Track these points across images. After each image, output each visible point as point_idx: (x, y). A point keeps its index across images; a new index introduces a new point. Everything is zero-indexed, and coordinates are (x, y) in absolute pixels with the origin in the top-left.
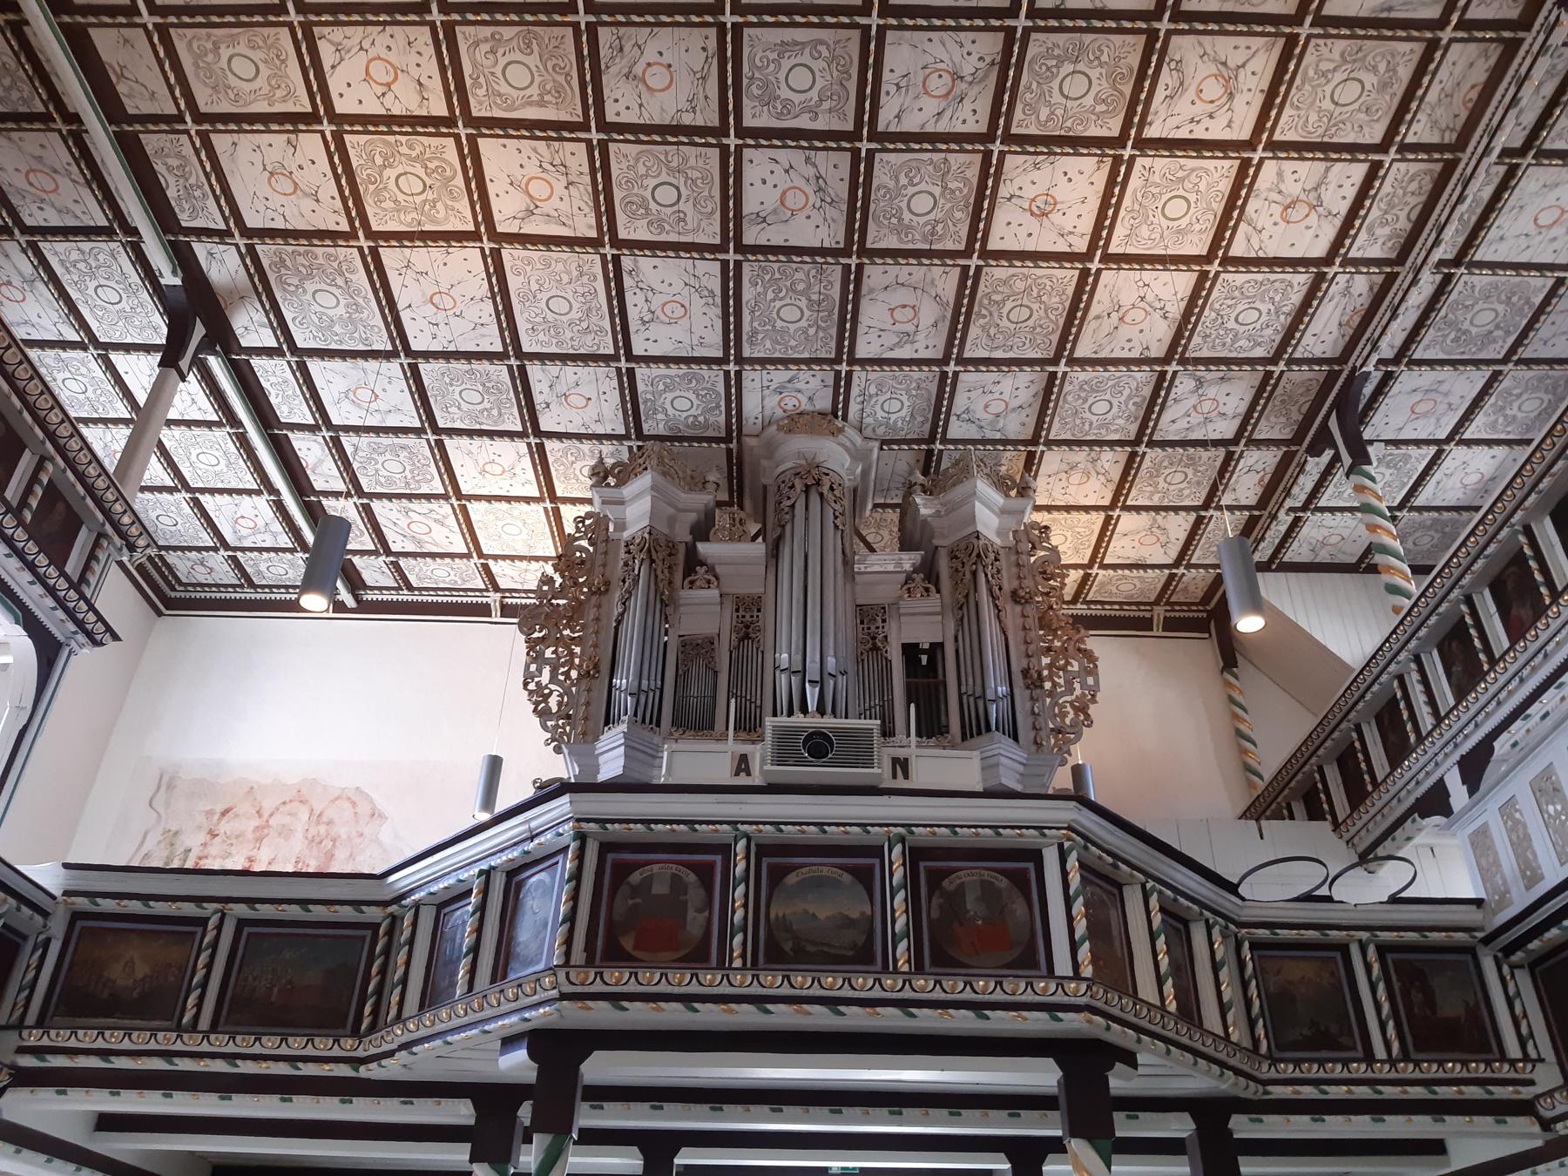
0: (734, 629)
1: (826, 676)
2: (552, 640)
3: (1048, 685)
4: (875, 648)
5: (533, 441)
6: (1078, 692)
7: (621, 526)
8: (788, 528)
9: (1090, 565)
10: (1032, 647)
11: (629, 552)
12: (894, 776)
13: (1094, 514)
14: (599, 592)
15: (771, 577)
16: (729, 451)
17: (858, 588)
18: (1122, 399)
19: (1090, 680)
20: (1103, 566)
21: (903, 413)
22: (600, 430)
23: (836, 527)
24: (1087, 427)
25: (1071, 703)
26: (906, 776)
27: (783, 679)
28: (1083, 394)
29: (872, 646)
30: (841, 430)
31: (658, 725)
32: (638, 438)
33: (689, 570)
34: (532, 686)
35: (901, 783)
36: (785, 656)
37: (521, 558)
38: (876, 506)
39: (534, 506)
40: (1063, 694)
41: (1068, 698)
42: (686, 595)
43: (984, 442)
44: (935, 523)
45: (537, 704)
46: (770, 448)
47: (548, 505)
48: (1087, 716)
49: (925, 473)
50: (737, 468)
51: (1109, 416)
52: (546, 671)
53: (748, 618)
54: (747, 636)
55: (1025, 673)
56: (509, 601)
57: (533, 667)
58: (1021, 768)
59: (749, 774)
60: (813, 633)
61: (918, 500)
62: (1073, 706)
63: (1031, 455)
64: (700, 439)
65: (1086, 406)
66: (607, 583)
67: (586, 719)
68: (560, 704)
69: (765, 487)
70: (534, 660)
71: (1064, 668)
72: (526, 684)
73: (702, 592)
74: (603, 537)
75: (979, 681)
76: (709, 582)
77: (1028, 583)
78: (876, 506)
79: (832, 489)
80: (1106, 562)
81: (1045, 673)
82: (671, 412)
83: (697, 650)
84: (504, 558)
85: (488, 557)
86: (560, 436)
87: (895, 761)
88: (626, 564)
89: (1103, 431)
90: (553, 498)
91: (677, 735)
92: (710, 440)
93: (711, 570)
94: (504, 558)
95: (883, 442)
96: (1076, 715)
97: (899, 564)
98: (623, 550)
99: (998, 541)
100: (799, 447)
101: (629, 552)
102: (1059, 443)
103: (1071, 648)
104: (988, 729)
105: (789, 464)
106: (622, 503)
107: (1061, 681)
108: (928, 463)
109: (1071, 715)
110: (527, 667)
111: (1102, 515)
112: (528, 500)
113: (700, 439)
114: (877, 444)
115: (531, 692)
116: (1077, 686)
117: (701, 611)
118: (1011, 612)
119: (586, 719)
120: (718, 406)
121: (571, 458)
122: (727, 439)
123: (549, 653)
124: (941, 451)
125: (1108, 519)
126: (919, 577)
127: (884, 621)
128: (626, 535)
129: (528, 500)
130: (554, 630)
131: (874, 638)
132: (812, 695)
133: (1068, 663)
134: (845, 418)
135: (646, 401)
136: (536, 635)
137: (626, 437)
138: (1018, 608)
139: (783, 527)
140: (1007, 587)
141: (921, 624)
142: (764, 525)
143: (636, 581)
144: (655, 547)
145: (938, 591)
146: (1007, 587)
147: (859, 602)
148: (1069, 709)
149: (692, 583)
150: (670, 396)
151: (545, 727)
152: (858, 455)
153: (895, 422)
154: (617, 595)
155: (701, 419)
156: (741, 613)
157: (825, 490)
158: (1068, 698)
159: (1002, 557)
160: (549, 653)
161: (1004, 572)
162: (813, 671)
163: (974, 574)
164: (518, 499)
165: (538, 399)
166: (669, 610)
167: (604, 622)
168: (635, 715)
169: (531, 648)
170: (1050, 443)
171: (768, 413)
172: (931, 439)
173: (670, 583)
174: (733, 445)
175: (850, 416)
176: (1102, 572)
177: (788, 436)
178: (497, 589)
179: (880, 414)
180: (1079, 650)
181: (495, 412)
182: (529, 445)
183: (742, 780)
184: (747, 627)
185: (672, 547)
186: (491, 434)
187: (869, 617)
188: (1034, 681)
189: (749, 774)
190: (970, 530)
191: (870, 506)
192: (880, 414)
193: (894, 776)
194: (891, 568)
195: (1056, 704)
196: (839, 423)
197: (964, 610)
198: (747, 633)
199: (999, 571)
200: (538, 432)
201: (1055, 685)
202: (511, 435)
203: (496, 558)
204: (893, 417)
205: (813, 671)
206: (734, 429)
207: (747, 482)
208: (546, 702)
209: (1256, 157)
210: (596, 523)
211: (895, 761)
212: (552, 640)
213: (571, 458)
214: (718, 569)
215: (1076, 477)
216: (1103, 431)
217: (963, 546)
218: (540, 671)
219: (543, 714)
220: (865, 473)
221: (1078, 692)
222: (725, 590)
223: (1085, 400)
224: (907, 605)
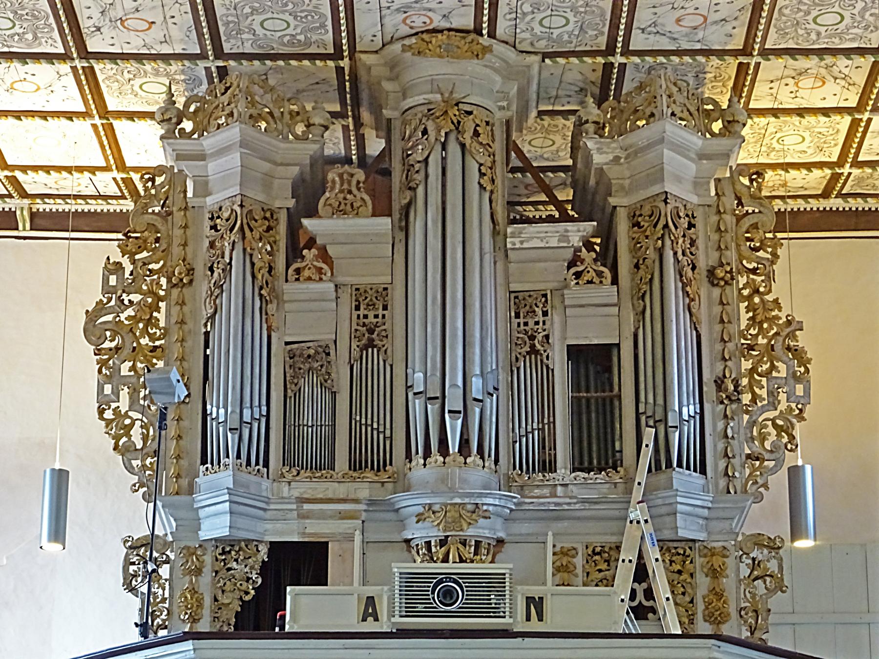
0: (354, 335)
1: (469, 402)
2: (127, 351)
3: (746, 398)
4: (533, 351)
5: (79, 64)
6: (783, 406)
7: (203, 189)
8: (420, 190)
9: (840, 163)
10: (731, 346)
11: (214, 227)
12: (528, 619)
13: (837, 118)
14: (180, 284)
15: (400, 248)
16: (340, 70)
17: (512, 266)
18: (855, 11)
19: (800, 389)
20: (857, 164)
21: (569, 28)
22: (166, 50)
23: (482, 187)
24: (813, 36)
25: (773, 420)
26: (540, 619)
27: (417, 405)
28: (805, 8)
29: (530, 348)
30: (487, 49)
31: (266, 465)
32: (217, 58)
33: (294, 252)
34: (108, 415)
35: (535, 626)
36: (419, 376)
37: (59, 169)
38: (541, 114)
39: (78, 122)
40: (764, 409)
41: (771, 414)
42: (291, 289)
43: (679, 53)
44: (613, 173)
45: (117, 438)
46: (394, 67)
47: (98, 121)
48: (792, 438)
49: (600, 101)
50: (354, 94)
51: (841, 27)
52: (124, 393)
53: (371, 319)
54: (371, 344)
55: (719, 384)
56: (41, 208)
57: (108, 389)
58: (705, 512)
59: (376, 619)
60: (454, 329)
61: (590, 144)
62: (775, 425)
63: (742, 69)
64: (299, 57)
65: (810, 18)
66: (190, 271)
67: (178, 457)
68: (145, 438)
69: (389, 121)
70: (109, 379)
71: (767, 374)
72: (101, 412)
73: (312, 286)
74: (180, 203)
75: (660, 401)
76: (320, 270)
77: (731, 255)
78: (541, 114)
79: (476, 134)
80: (861, 158)
81: (745, 381)
82: (260, 31)
83: (308, 360)
84: (36, 168)
85: (13, 168)
86: (113, 57)
87: (529, 600)
88: (212, 245)
89: (837, 40)
90: (105, 113)
91: (289, 477)
92: (312, 57)
93: (324, 255)
94: (36, 168)
95: (545, 55)
96: (779, 435)
97: (564, 237)
98: (208, 223)
99: (694, 199)
100: (431, 70)
101: (214, 227)
102: (779, 52)
103: (778, 347)
104: (669, 465)
105: (420, 99)
106: (202, 157)
107: (764, 393)
108: (606, 87)
109: (773, 437)
110: (100, 389)
111: (846, 121)
112: (70, 116)
113: (299, 57)
114: (538, 58)
115: (109, 422)
116: (783, 397)
117: (314, 311)
118: (704, 292)
119: (178, 457)
120: (323, 26)
121: (127, 76)
122: (337, 55)
123: (125, 369)
124: (622, 66)
125: (854, 124)
126: (588, 256)
127: (545, 314)
128: (211, 201)
129: (70, 116)
130: (129, 338)
131: (532, 338)
132: (454, 428)
133: (773, 367)
134: (492, 35)
135: (227, 24)
136: (107, 345)
137: (203, 56)
138: (716, 292)
139: (413, 189)
140: (703, 264)
141: (592, 316)
142: (389, 142)
143: (227, 270)
144: (251, 221)
145: (615, 281)
146: (703, 264)
147: (514, 287)
148: (771, 429)
149: (298, 271)
150: (259, 18)
151: (130, 469)
152: (508, 72)
153: (560, 36)
154: (205, 288)
155: (302, 38)
156: (362, 312)
157: (467, 138)
158: (771, 414)
159: (699, 222)
160: (125, 369)
161: (700, 243)
162: (454, 401)
163: (661, 252)
164: (37, 57)
165: (85, 24)
166: (272, 308)
167: (190, 325)
168: (239, 456)
169: (102, 364)
170: (765, 53)
171: (389, 30)
172: (610, 50)
173: (271, 269)
174: (345, 63)
175: (500, 32)
176: (856, 172)
177: (417, 59)
178: (24, 194)
179: (538, 29)
180: (789, 349)
181: (29, 36)
182: (74, 69)
183: (370, 626)
184: (371, 331)
185: (270, 215)
186: (23, 57)
187: (523, 305)
188: (728, 392)
189: (376, 619)
190: (656, 189)
191: (534, 114)
192: (538, 29)
193: (528, 619)
194: (554, 243)
195: (755, 422)
196: (485, 40)
197: (646, 297)
198: (370, 339)
199: (693, 243)
200: (85, 54)
201: (754, 400)
202: (50, 58)
203: (24, 169)
204: (556, 32)
205: (454, 401)
206: (345, 46)
207: (363, 86)
208: (129, 436)
209: (866, 116)
210: (170, 182)
211: (529, 600)
212: (127, 351)
213: (127, 76)
214: (331, 250)
215: (806, 82)
216: (837, 40)
217: (646, 211)
218: (116, 393)
219: (125, 451)
220: (522, 92)
221: (783, 406)
222: (340, 279)
223: (808, 13)
224: (576, 293)
